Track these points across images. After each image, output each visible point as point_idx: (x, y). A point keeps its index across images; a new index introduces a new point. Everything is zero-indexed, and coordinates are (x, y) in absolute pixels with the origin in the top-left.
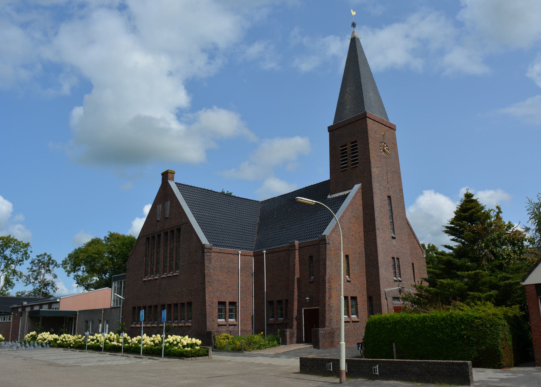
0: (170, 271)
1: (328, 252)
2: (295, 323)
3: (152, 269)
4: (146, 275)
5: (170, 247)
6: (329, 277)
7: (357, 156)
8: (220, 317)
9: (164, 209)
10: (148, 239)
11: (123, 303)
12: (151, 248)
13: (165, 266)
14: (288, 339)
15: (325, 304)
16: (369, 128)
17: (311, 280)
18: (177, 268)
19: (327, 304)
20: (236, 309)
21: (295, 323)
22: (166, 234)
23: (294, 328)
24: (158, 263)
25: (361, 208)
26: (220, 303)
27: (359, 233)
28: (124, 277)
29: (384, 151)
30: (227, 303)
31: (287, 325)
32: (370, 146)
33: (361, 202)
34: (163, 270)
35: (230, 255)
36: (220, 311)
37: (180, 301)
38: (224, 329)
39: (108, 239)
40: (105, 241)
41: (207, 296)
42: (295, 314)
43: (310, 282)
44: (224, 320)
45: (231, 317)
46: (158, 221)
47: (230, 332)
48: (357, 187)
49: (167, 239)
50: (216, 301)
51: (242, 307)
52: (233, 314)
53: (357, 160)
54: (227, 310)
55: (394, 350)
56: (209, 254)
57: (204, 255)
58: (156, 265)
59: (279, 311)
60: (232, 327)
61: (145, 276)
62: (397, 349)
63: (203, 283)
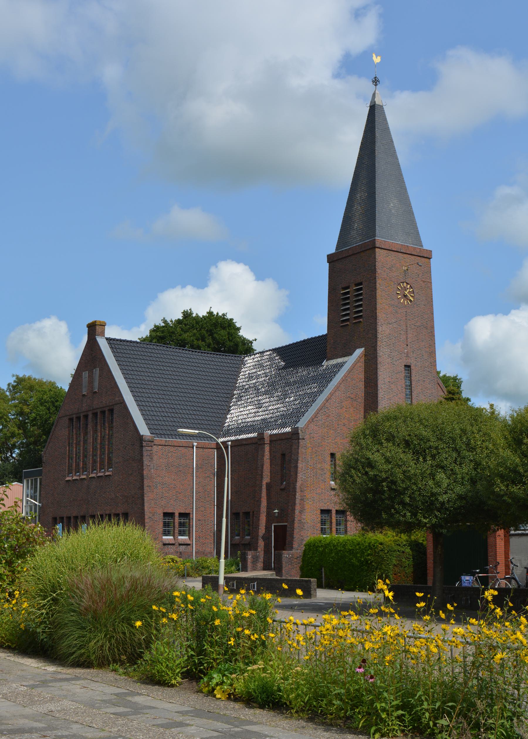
0: (101, 469)
1: (301, 450)
2: (261, 544)
3: (77, 465)
4: (70, 472)
5: (101, 434)
6: (302, 485)
7: (360, 306)
8: (166, 533)
9: (91, 377)
10: (71, 420)
11: (39, 509)
12: (76, 434)
13: (94, 462)
14: (249, 564)
15: (294, 520)
16: (378, 265)
17: (283, 487)
18: (110, 465)
19: (296, 519)
20: (189, 522)
21: (261, 544)
22: (95, 415)
23: (259, 550)
24: (85, 456)
25: (362, 385)
26: (166, 514)
27: (355, 421)
28: (40, 473)
29: (405, 296)
30: (177, 515)
31: (251, 546)
32: (379, 293)
33: (362, 376)
34: (92, 467)
35: (180, 449)
36: (166, 525)
37: (113, 511)
38: (171, 549)
39: (14, 387)
40: (10, 391)
41: (146, 505)
42: (262, 531)
43: (281, 489)
44: (172, 537)
45: (181, 533)
46: (84, 395)
47: (180, 555)
48: (359, 352)
49: (97, 423)
50: (160, 512)
51: (198, 520)
52: (185, 527)
53: (361, 311)
54: (177, 524)
55: (323, 576)
56: (149, 448)
57: (142, 450)
58: (83, 459)
59: (247, 527)
60: (184, 547)
61: (69, 473)
62: (325, 575)
63: (142, 488)
